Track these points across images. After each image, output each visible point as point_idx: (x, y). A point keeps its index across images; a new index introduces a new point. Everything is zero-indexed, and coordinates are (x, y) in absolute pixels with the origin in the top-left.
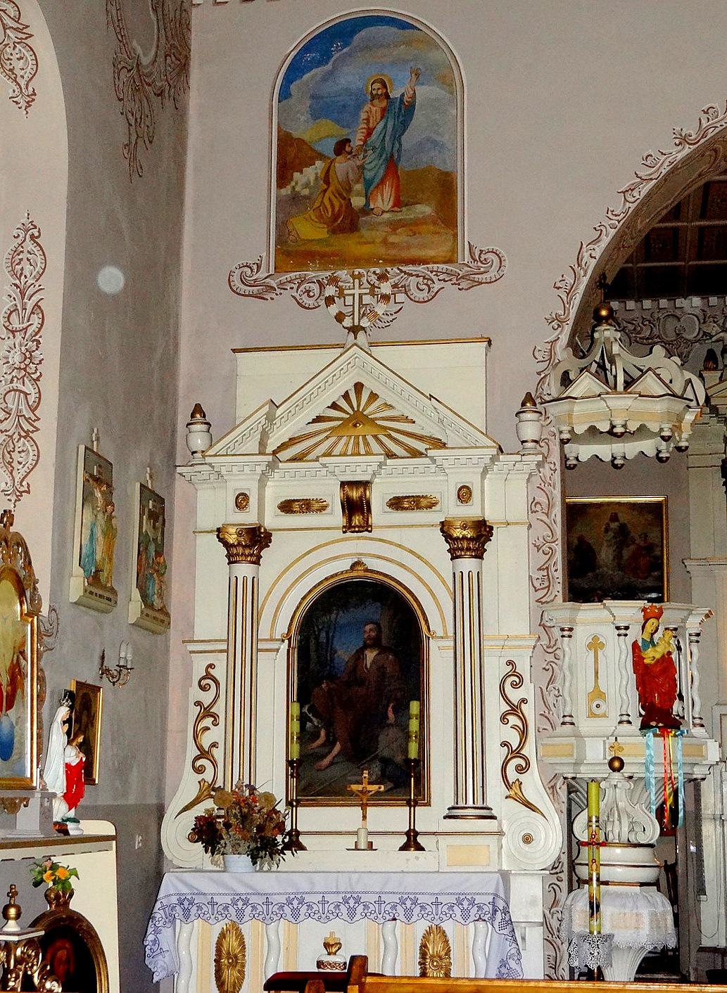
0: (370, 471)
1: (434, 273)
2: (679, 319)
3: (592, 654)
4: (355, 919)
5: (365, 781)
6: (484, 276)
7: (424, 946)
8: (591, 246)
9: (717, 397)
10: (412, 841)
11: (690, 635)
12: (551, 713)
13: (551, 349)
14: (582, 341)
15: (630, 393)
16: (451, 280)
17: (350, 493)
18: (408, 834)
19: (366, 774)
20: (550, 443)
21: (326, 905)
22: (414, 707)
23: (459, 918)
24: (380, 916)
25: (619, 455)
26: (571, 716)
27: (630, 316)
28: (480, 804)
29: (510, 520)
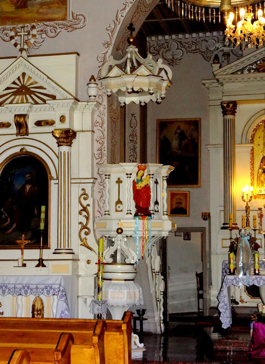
0: (26, 110)
1: (57, 25)
2: (207, 42)
3: (118, 185)
4: (5, 294)
5: (23, 239)
6: (77, 26)
7: (34, 306)
8: (122, 12)
9: (219, 75)
10: (41, 263)
11: (163, 177)
12: (101, 210)
13: (104, 57)
14: (119, 52)
15: (133, 75)
16: (64, 28)
17: (18, 119)
18: (39, 260)
19: (23, 236)
20: (103, 97)
21: (16, 289)
22: (43, 208)
23: (46, 294)
24: (15, 293)
25: (143, 101)
26: (108, 211)
27: (186, 41)
28: (67, 248)
29: (84, 129)
